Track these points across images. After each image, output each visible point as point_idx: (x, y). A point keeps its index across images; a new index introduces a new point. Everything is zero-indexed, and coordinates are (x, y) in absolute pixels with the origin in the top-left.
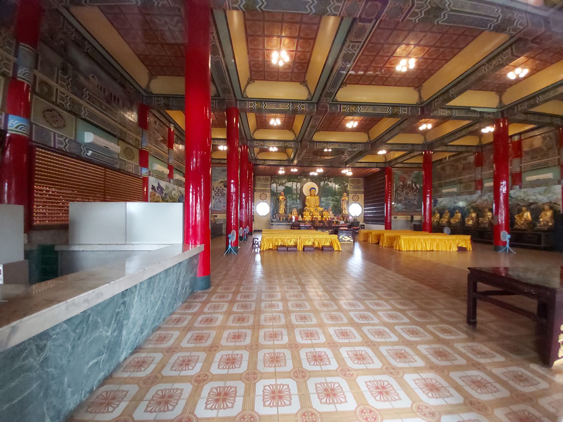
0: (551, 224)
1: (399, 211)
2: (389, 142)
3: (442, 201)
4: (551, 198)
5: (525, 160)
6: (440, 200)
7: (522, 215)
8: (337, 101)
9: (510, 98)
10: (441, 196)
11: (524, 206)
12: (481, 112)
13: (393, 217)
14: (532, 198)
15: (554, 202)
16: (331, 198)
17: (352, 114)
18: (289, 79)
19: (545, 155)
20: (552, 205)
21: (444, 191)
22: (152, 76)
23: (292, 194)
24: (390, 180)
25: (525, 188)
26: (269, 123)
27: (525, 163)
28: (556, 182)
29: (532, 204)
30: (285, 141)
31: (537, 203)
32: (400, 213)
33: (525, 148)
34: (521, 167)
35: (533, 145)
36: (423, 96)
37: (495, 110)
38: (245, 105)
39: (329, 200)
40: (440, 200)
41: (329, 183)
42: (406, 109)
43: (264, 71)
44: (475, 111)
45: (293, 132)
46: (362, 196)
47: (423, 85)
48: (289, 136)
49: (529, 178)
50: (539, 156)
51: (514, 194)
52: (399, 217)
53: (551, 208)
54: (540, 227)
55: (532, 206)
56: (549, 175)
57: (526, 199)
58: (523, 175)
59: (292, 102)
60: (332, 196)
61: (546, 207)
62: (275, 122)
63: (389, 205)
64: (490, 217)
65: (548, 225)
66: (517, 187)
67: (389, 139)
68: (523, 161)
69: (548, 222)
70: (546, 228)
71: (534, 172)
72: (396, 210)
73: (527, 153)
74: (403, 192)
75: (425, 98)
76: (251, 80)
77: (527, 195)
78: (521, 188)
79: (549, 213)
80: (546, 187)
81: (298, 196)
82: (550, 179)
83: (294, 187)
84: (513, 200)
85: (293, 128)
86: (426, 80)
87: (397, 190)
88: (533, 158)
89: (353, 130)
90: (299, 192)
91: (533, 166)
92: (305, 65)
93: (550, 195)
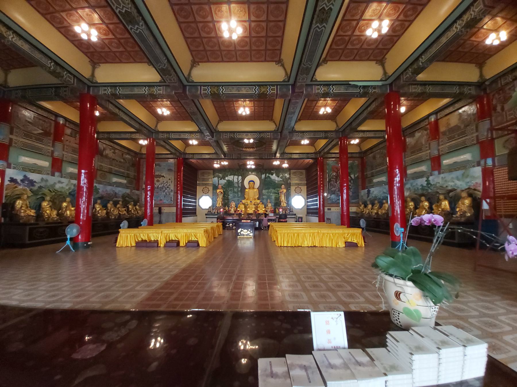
0: (469, 215)
1: (333, 203)
2: (361, 128)
3: (373, 192)
4: (469, 184)
5: (442, 141)
6: (372, 190)
7: (441, 204)
8: (316, 81)
9: (493, 68)
10: (372, 187)
11: (442, 194)
12: (364, 87)
13: (326, 209)
14: (450, 185)
15: (473, 188)
16: (273, 191)
17: (325, 95)
18: (263, 59)
19: (463, 134)
20: (471, 191)
21: (375, 180)
22: (94, 64)
23: (234, 187)
24: (322, 170)
25: (443, 173)
26: (237, 112)
27: (442, 145)
28: (476, 164)
29: (451, 191)
30: (260, 132)
31: (456, 190)
32: (334, 205)
33: (442, 129)
34: (438, 150)
35: (450, 124)
36: (387, 71)
37: (380, 84)
38: (99, 91)
39: (271, 192)
40: (372, 190)
41: (270, 176)
42: (162, 88)
43: (220, 50)
44: (356, 86)
45: (274, 122)
46: (304, 188)
47: (386, 57)
48: (267, 126)
49: (446, 162)
50: (456, 136)
51: (433, 180)
52: (333, 209)
53: (470, 195)
54: (456, 219)
55: (451, 194)
56: (466, 156)
57: (445, 186)
58: (442, 158)
59: (258, 85)
60: (274, 189)
61: (464, 194)
62: (244, 110)
63: (321, 197)
64: (412, 207)
65: (465, 216)
66: (436, 172)
67: (359, 124)
68: (440, 143)
69: (465, 212)
70: (463, 220)
71: (456, 153)
72: (330, 202)
73: (444, 133)
74: (336, 182)
75: (390, 72)
76: (194, 63)
77: (446, 181)
78: (439, 173)
79: (467, 202)
80: (463, 171)
81: (239, 189)
82: (469, 160)
83: (236, 180)
84: (432, 188)
85: (274, 118)
86: (389, 50)
87: (330, 181)
88: (451, 139)
89: (326, 117)
90: (240, 185)
91: (450, 147)
92: (279, 39)
93: (468, 180)
